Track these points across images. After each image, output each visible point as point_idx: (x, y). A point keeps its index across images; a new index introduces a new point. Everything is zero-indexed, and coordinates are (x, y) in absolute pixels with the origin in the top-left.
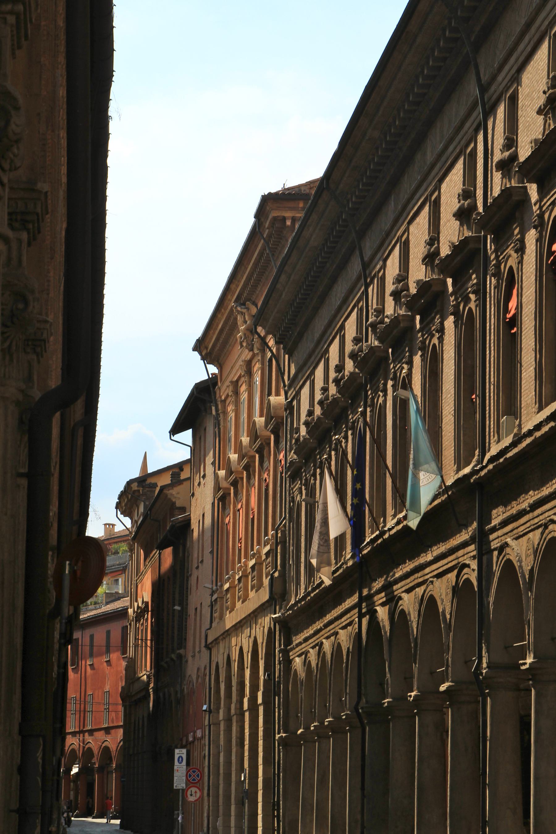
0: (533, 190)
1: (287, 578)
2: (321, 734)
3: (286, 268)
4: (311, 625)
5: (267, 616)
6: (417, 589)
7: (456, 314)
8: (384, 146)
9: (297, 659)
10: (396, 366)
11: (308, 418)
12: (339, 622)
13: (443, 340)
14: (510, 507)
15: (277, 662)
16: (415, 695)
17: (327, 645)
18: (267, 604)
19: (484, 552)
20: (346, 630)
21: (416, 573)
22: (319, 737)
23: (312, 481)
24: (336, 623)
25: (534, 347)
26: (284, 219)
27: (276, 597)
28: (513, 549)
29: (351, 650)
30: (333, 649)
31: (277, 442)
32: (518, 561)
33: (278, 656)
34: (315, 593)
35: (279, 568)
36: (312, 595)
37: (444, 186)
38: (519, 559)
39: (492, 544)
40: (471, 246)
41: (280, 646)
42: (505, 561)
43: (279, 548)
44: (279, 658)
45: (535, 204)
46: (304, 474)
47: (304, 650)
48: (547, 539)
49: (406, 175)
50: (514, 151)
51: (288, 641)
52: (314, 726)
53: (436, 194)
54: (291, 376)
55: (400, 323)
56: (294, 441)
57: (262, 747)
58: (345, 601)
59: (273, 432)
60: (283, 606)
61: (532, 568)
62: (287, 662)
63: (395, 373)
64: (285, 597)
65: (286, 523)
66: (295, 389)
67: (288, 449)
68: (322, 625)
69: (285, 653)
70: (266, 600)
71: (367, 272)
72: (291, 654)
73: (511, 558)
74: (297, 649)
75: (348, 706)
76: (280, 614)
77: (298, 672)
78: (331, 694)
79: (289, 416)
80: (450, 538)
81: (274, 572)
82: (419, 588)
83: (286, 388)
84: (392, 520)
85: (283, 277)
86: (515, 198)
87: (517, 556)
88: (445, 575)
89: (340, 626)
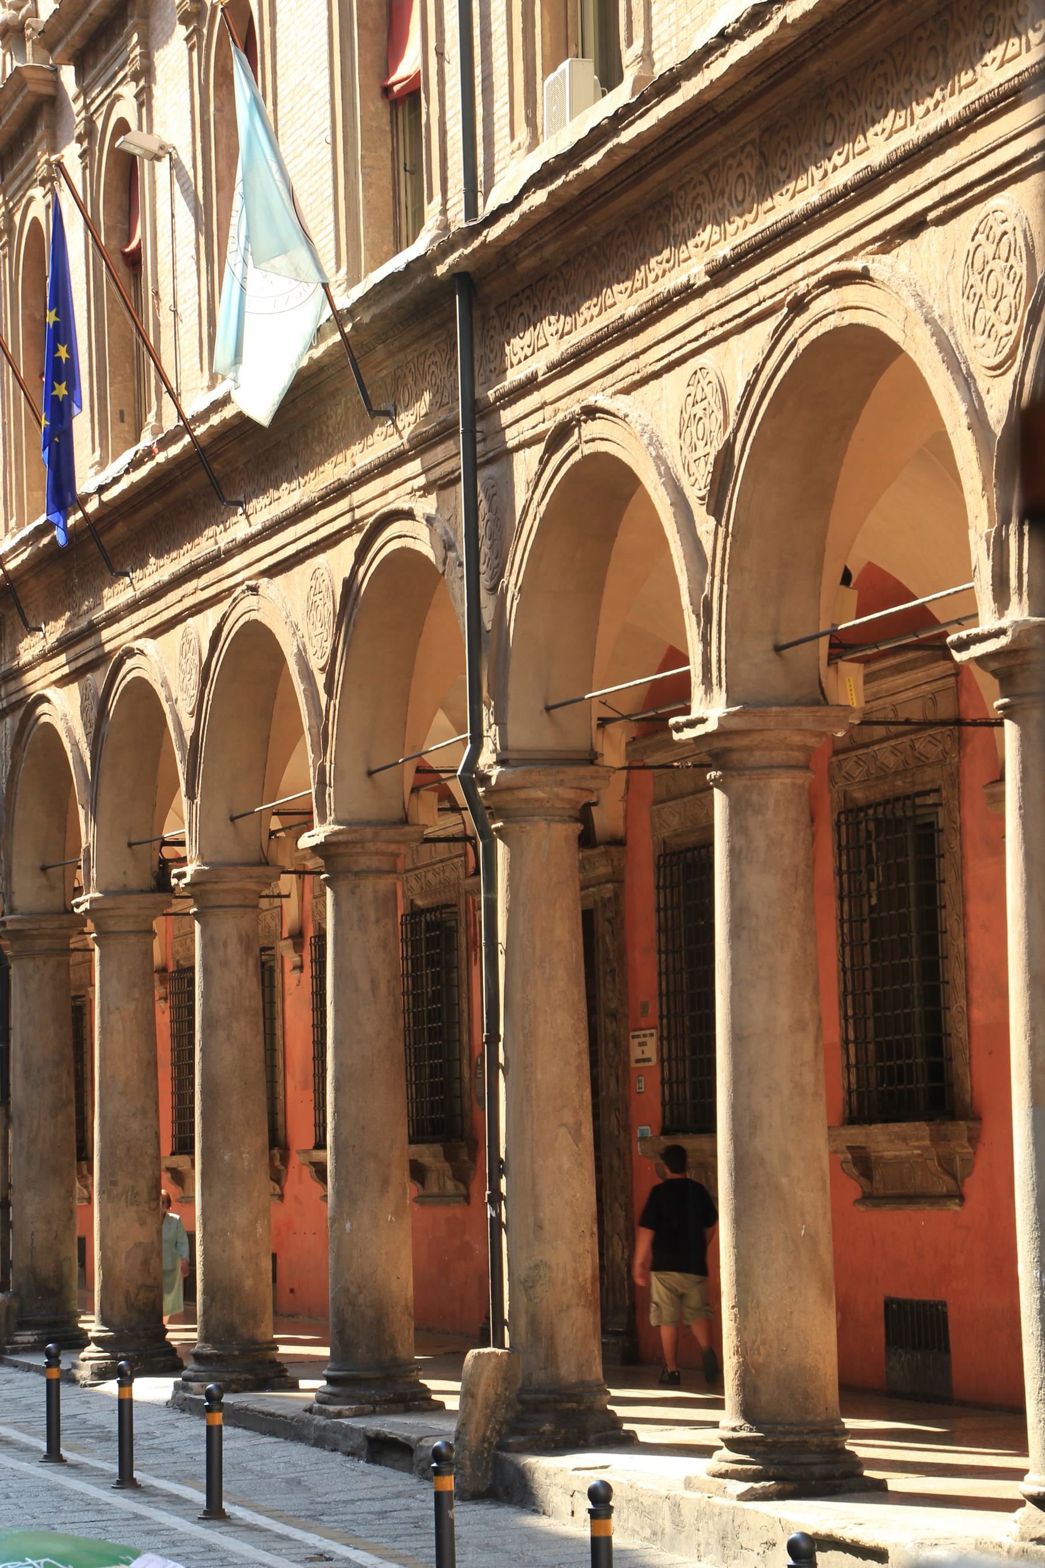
0: (68, 75)
6: (190, 621)
13: (150, 96)
14: (595, 311)
19: (478, 461)
21: (190, 580)
28: (626, 416)
38: (651, 438)
39: (509, 433)
42: (575, 465)
45: (76, 99)
61: (728, 448)
63: (90, 121)
80: (321, 463)
88: (173, 627)
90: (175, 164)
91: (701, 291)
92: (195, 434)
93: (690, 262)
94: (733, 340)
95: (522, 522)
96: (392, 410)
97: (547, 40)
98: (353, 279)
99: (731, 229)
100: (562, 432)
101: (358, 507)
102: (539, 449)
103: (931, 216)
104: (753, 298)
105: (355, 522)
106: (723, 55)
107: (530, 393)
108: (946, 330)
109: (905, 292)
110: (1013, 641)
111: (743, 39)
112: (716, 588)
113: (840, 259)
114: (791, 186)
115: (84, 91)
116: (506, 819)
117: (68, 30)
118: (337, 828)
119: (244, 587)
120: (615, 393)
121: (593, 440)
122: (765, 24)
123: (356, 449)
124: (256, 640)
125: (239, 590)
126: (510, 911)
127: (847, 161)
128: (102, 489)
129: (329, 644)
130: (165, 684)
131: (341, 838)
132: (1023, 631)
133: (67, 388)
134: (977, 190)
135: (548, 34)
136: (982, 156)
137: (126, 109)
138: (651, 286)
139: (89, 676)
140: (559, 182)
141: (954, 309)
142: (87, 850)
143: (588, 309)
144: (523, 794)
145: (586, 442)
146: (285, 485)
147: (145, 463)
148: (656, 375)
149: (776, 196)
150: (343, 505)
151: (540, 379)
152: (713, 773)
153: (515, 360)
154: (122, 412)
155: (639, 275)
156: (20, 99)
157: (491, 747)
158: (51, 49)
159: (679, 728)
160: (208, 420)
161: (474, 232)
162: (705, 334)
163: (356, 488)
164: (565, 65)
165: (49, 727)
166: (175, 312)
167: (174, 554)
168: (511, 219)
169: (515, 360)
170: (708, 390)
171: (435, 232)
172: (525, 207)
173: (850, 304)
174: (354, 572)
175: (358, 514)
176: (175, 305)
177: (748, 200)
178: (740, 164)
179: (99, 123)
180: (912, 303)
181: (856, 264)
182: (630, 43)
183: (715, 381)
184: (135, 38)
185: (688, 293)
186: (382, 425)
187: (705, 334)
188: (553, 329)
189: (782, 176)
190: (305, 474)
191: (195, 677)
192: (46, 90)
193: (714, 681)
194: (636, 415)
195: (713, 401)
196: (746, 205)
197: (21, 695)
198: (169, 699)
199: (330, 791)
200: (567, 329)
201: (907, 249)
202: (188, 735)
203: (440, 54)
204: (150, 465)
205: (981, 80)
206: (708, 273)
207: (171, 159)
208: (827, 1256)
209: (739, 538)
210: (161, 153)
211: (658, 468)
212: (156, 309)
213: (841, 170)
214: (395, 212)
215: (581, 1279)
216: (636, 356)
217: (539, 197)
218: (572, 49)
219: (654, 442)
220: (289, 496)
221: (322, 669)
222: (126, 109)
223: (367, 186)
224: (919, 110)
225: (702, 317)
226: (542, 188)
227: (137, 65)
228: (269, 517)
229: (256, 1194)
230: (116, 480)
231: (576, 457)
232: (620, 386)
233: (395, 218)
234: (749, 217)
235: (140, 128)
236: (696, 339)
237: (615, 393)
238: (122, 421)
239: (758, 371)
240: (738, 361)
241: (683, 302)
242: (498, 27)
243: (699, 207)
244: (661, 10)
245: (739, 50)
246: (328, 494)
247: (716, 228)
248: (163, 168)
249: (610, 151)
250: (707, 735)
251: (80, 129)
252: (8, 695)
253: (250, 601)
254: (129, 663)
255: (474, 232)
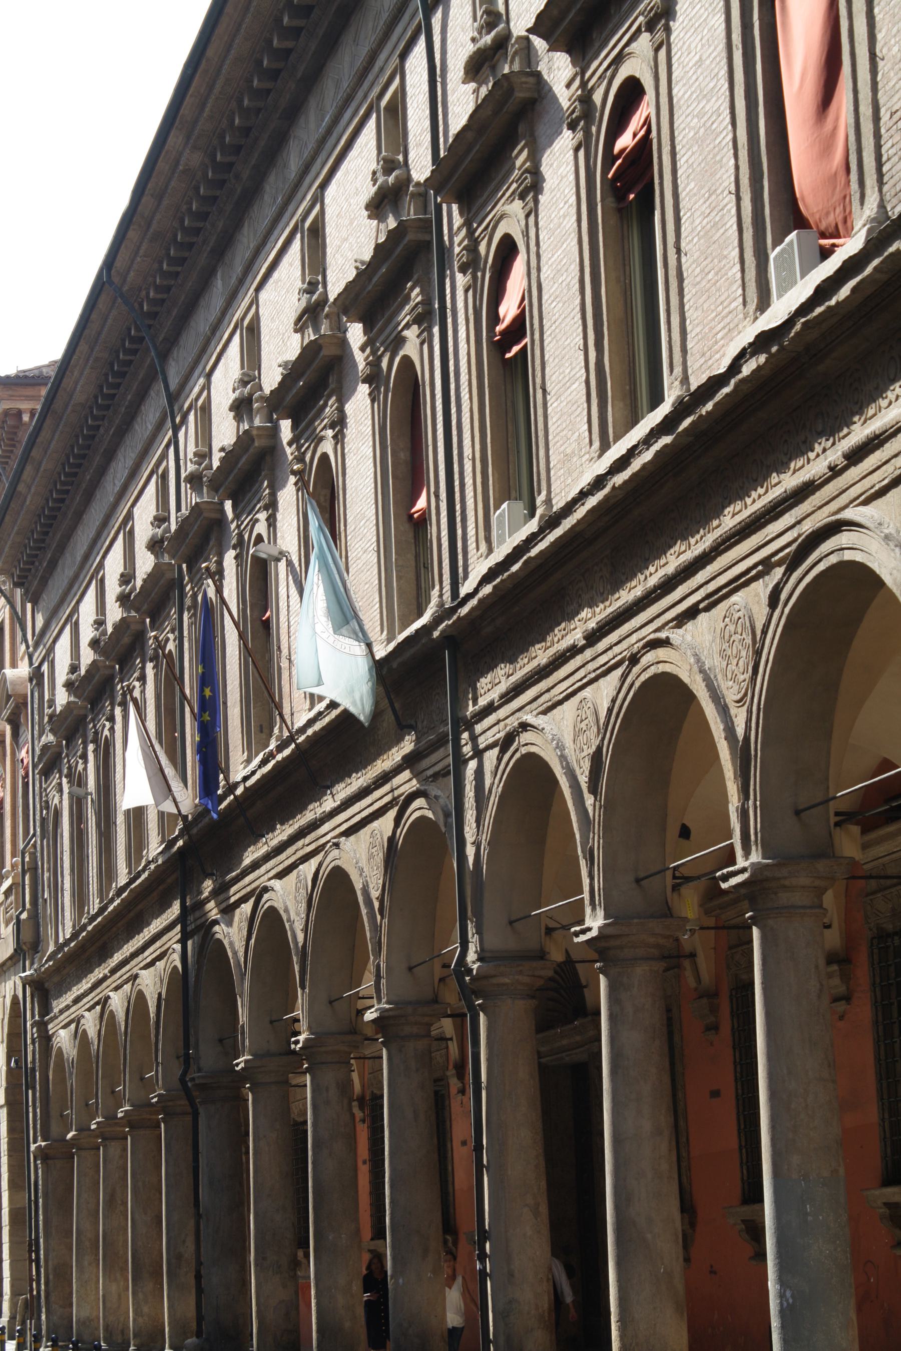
0: (228, 505)
1: (41, 920)
2: (111, 1134)
3: (34, 453)
4: (86, 976)
5: (10, 979)
6: (301, 867)
7: (374, 378)
8: (210, 174)
9: (62, 1032)
10: (242, 523)
11: (70, 675)
12: (140, 958)
14: (526, 660)
15: (29, 1041)
16: (307, 1040)
17: (117, 1002)
18: (10, 962)
20: (152, 969)
21: (300, 839)
22: (104, 1139)
23: (80, 767)
24: (133, 963)
25: (582, 341)
26: (19, 413)
27: (24, 947)
28: (543, 729)
29: (164, 996)
30: (129, 1002)
31: (16, 735)
32: (557, 748)
33: (31, 1032)
34: (95, 923)
35: (28, 906)
36: (90, 928)
37: (331, 192)
38: (558, 744)
40: (411, 236)
41: (33, 1016)
42: (518, 761)
43: (27, 877)
44: (33, 1035)
45: (232, 521)
46: (66, 760)
47: (73, 1016)
48: (637, 684)
49: (246, 224)
50: (503, 28)
51: (45, 1009)
52: (97, 1123)
53: (318, 207)
54: (37, 630)
55: (253, 440)
56: (46, 719)
57: (6, 1166)
58: (149, 924)
59: (10, 721)
60: (36, 960)
61: (599, 749)
62: (46, 1039)
63: (240, 536)
64: (37, 946)
65: (35, 842)
66: (45, 646)
67: (36, 736)
68: (106, 971)
69: (42, 1026)
70: (8, 955)
71: (176, 408)
72: (50, 1027)
73: (276, 905)
74: (62, 1017)
75: (160, 1082)
76: (32, 971)
77: (65, 1052)
78: (127, 1070)
79: (36, 689)
80: (375, 760)
81: (21, 913)
82: (306, 864)
83: (31, 649)
84: (244, 768)
85: (29, 469)
86: (520, 95)
87: (553, 739)
88: (291, 871)
89: (142, 965)
90: (289, 563)
91: (582, 650)
92: (298, 741)
93: (572, 633)
94: (601, 681)
95: (489, 798)
96: (414, 724)
97: (497, 489)
98: (389, 641)
99: (598, 610)
100: (509, 740)
101: (396, 789)
102: (496, 750)
103: (702, 606)
104: (610, 654)
105: (394, 799)
106: (583, 504)
107: (490, 714)
108: (712, 677)
109: (689, 653)
110: (751, 876)
111: (593, 495)
112: (596, 842)
113: (655, 631)
114: (628, 585)
115: (237, 516)
116: (485, 998)
117: (226, 478)
118: (387, 1006)
119: (331, 844)
120: (538, 714)
121: (526, 744)
122: (604, 487)
123: (394, 750)
124: (339, 876)
125: (329, 845)
126: (489, 1060)
127: (657, 570)
128: (245, 779)
129: (381, 881)
130: (286, 910)
131: (391, 1013)
132: (757, 869)
133: (209, 715)
134: (724, 591)
135: (497, 486)
136: (725, 571)
137: (261, 528)
138: (556, 645)
139: (243, 905)
140: (498, 580)
141: (716, 664)
142: (243, 1025)
143: (522, 660)
144: (495, 981)
145: (523, 746)
146: (354, 775)
147: (269, 761)
148: (560, 703)
149: (621, 591)
150: (386, 788)
151: (496, 704)
152: (598, 964)
153: (482, 692)
154: (261, 726)
155: (549, 639)
156: (199, 522)
157: (474, 949)
158: (216, 490)
159: (577, 934)
160: (305, 732)
161: (453, 610)
162: (585, 677)
163: (394, 776)
164: (505, 505)
165: (219, 941)
166: (290, 659)
167: (291, 822)
168: (474, 602)
169: (482, 692)
170: (588, 712)
171: (435, 609)
172: (480, 595)
173: (661, 659)
174: (394, 832)
175: (396, 793)
176: (290, 655)
177: (606, 592)
178: (601, 570)
179: (246, 537)
180: (692, 660)
181: (663, 635)
182: (539, 493)
183: (592, 707)
184: (266, 483)
185: (574, 651)
186: (409, 735)
187: (585, 677)
188: (503, 672)
189: (623, 578)
190: (365, 768)
191: (304, 905)
192: (214, 515)
193: (597, 902)
194: (549, 728)
195: (591, 719)
196: (605, 595)
197: (203, 920)
198: (289, 920)
199: (383, 981)
200: (511, 672)
201: (690, 626)
202: (300, 944)
203: (437, 496)
204: (273, 762)
205: (723, 525)
206: (585, 638)
207: (287, 560)
208: (680, 1287)
209: (608, 808)
210: (280, 556)
211: (561, 763)
212: (279, 657)
213: (653, 575)
214: (418, 594)
215: (540, 1310)
216: (548, 690)
217: (487, 589)
218: (513, 494)
219: (560, 747)
220: (358, 781)
221: (377, 898)
222: (261, 528)
223: (399, 578)
224: (692, 541)
225: (583, 666)
226: (489, 583)
227: (267, 500)
228: (344, 796)
229: (351, 1263)
230: (253, 773)
231: (518, 755)
232: (541, 709)
233: (418, 598)
234: (607, 603)
235: (269, 542)
236: (581, 680)
237: (538, 714)
238: (261, 732)
239: (614, 701)
240: (604, 693)
241: (573, 656)
242: (469, 480)
243: (580, 596)
244: (555, 473)
245: (592, 502)
246: (377, 781)
247: (589, 610)
248: (282, 565)
249: (526, 561)
250: (593, 939)
251: (234, 541)
252: (195, 920)
253: (335, 853)
254: (266, 896)
255: (453, 610)
